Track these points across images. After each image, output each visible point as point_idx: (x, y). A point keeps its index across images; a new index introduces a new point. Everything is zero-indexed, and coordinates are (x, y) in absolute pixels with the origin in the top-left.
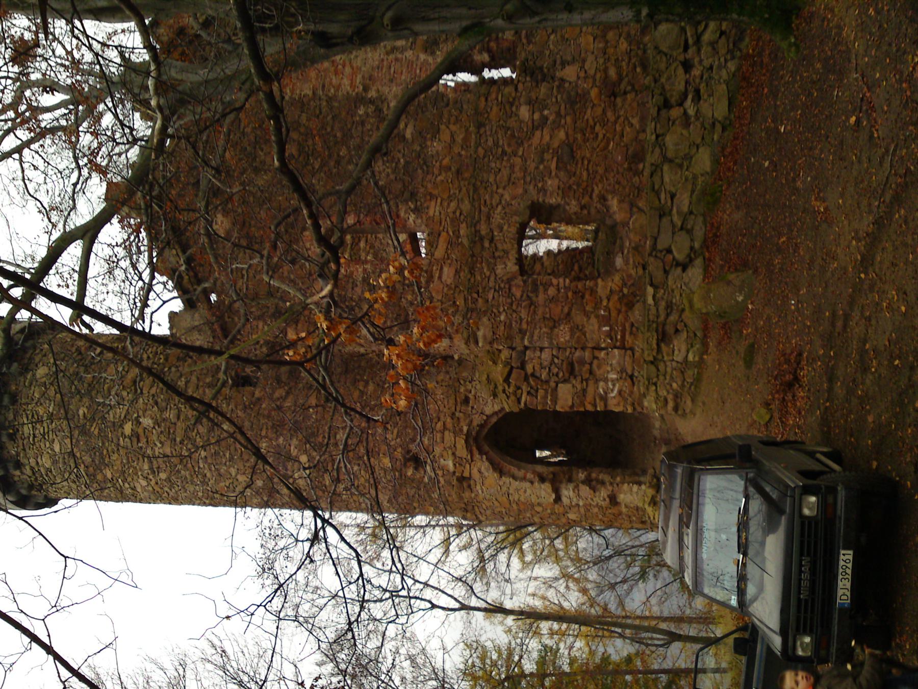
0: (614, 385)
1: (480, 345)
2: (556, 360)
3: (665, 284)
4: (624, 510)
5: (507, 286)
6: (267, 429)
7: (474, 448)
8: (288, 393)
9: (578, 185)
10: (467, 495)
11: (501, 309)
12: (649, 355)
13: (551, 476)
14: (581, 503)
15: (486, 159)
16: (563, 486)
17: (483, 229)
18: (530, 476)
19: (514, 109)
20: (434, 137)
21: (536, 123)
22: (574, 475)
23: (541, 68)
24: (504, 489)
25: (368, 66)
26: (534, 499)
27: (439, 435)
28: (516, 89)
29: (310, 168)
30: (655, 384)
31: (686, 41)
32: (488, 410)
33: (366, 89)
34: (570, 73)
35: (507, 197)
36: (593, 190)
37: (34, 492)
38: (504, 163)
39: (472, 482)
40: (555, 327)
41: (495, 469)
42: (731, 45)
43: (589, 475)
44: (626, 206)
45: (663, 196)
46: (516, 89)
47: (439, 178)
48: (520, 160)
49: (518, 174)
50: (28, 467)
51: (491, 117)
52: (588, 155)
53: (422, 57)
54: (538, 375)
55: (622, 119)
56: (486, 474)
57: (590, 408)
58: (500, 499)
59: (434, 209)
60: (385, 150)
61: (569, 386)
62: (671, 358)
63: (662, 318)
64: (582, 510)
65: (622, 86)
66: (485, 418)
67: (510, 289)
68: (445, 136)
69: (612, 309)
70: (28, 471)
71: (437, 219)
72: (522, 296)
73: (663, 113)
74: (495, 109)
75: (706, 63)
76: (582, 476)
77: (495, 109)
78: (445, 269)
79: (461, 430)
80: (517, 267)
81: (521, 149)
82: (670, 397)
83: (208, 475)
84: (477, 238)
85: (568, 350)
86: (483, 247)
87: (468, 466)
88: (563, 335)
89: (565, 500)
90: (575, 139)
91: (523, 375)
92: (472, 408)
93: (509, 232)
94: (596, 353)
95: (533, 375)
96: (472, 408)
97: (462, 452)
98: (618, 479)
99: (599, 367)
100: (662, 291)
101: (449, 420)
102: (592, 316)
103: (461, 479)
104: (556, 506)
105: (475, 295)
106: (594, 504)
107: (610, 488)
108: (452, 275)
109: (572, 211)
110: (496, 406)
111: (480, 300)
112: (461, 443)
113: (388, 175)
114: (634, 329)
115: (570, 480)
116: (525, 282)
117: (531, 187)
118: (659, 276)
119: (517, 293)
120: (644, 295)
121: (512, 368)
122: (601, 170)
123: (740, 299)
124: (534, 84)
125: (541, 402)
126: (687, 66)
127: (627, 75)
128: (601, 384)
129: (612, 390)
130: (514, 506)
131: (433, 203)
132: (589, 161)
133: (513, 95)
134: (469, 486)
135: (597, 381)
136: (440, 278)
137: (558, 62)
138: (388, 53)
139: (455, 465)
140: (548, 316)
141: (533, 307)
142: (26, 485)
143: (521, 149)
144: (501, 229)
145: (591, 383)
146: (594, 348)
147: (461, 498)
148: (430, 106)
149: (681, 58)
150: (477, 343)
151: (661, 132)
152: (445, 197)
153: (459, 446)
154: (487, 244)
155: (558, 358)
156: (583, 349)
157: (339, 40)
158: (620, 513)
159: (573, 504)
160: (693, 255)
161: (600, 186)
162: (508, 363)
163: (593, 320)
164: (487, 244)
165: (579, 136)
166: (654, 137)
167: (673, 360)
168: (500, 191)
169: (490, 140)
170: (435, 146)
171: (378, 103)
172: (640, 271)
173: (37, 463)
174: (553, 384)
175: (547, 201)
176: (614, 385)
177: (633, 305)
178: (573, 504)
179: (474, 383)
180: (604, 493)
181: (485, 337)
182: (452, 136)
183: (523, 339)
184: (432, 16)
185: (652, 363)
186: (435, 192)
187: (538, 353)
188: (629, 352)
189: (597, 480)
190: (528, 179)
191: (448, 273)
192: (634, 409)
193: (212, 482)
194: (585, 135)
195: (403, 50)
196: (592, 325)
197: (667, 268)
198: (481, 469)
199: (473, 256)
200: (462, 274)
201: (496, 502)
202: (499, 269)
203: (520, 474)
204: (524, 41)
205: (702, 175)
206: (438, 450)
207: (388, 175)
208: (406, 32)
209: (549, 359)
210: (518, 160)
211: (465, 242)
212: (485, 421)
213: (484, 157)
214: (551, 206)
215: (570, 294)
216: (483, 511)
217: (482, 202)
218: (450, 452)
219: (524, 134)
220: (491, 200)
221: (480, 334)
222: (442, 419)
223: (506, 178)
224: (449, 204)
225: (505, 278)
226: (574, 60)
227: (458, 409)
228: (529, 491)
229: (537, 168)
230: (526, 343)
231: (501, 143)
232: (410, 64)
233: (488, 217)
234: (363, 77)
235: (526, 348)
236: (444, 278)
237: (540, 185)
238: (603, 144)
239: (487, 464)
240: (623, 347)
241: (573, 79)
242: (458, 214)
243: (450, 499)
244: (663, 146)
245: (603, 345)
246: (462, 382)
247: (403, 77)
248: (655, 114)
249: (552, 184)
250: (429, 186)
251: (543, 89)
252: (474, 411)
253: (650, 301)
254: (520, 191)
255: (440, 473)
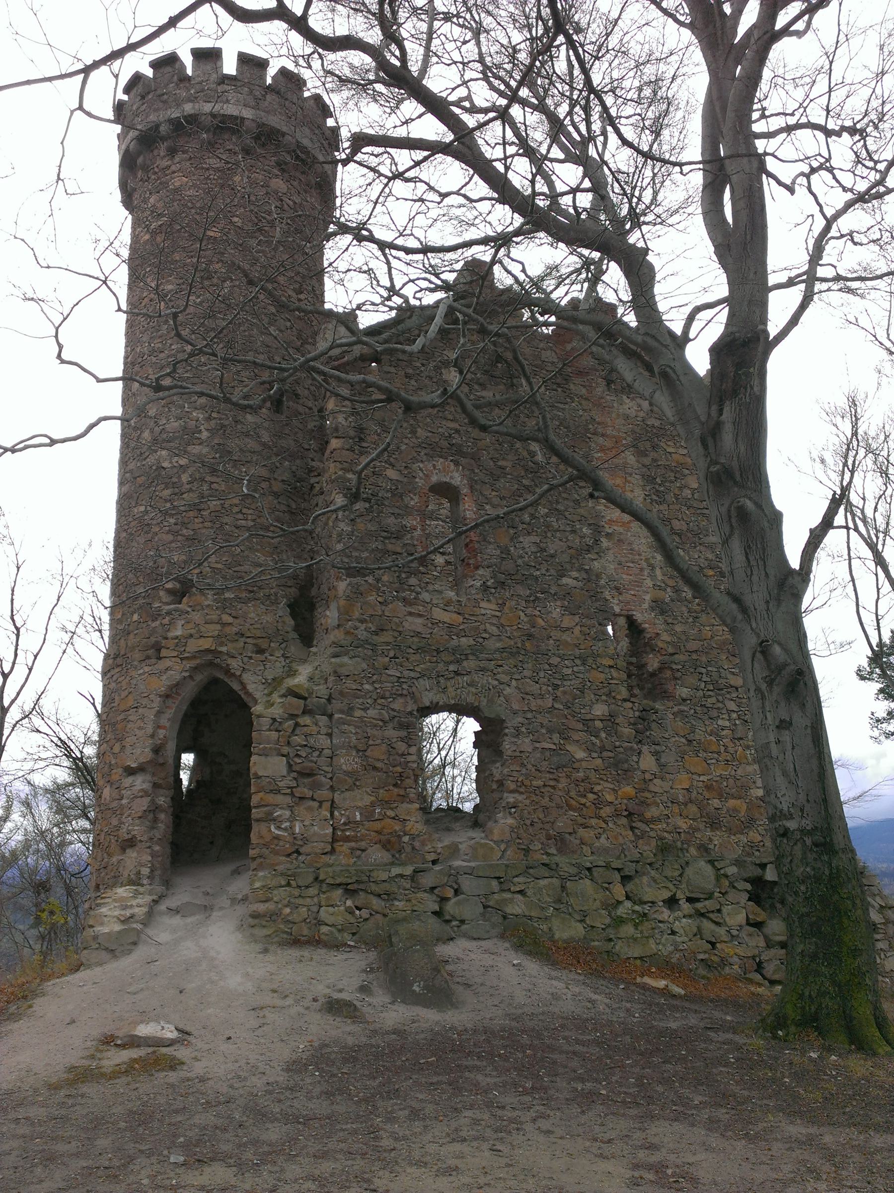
0: (285, 829)
1: (333, 660)
2: (316, 754)
3: (417, 888)
4: (114, 859)
5: (405, 692)
6: (220, 419)
7: (198, 661)
8: (264, 445)
9: (527, 776)
10: (137, 655)
11: (377, 686)
12: (327, 873)
13: (161, 761)
14: (124, 801)
15: (547, 667)
16: (148, 777)
17: (470, 664)
18: (162, 733)
19: (604, 698)
20: (566, 608)
21: (590, 723)
22: (162, 791)
23: (650, 729)
24: (145, 702)
25: (633, 539)
26: (129, 740)
27: (214, 617)
28: (625, 700)
29: (523, 474)
30: (289, 884)
31: (697, 900)
32: (247, 677)
33: (608, 535)
34: (648, 762)
35: (508, 691)
36: (522, 793)
37: (140, 174)
38: (544, 688)
39: (153, 661)
40: (358, 751)
41: (171, 688)
42: (701, 956)
43: (163, 811)
44: (507, 836)
45: (520, 879)
46: (625, 700)
47: (522, 614)
48: (550, 705)
49: (533, 705)
50: (169, 163)
51: (594, 672)
52: (560, 786)
53: (648, 597)
54: (297, 732)
55: (604, 825)
56: (164, 677)
57: (255, 800)
58: (130, 697)
59: (488, 608)
60: (596, 494)
61: (284, 772)
62: (323, 903)
63: (374, 887)
64: (114, 804)
65: (639, 824)
66: (238, 673)
67: (401, 695)
68: (567, 622)
69: (383, 823)
70: (165, 163)
71: (478, 611)
72: (393, 710)
73: (617, 876)
74: (602, 676)
75: (677, 926)
76: (162, 801)
77: (602, 676)
78: (419, 621)
79: (222, 644)
80: (428, 704)
81: (561, 707)
82: (270, 906)
83: (162, 355)
84: (460, 656)
85: (329, 769)
86: (449, 663)
87: (175, 654)
88: (347, 762)
89: (128, 781)
90: (577, 770)
91: (296, 713)
92: (251, 658)
93: (468, 694)
94: (327, 805)
95: (297, 725)
96: (251, 658)
97: (193, 646)
98: (157, 848)
99: (310, 809)
100: (408, 886)
101: (235, 629)
102: (373, 798)
103: (158, 647)
104: (120, 770)
105: (392, 654)
106: (123, 819)
107: (145, 838)
108: (413, 627)
109: (495, 771)
110: (254, 686)
111: (387, 659)
112: (206, 644)
113: (521, 557)
114: (359, 852)
115: (156, 786)
116: (411, 713)
117: (520, 719)
118: (427, 880)
119: (397, 705)
120: (403, 864)
121: (305, 699)
122: (545, 801)
123: (416, 988)
124: (632, 720)
125: (264, 735)
126: (672, 902)
127: (652, 829)
128: (288, 813)
129: (279, 828)
130: (122, 717)
131: (494, 607)
132: (553, 787)
133: (618, 697)
134: (148, 658)
135: (291, 808)
136: (410, 614)
137: (657, 748)
138: (647, 560)
139: (177, 638)
140: (371, 742)
141: (381, 723)
142: (148, 162)
143: (561, 707)
144: (471, 684)
145: (288, 799)
146: (333, 801)
147: (133, 649)
148: (597, 604)
149: (679, 895)
150: (336, 656)
151: (595, 874)
152: (503, 621)
153: (201, 642)
154: (452, 668)
155: (319, 756)
156: (332, 788)
157: (711, 449)
158: (110, 855)
159: (123, 792)
160: (454, 923)
161: (527, 802)
162: (311, 694)
163: (368, 800)
164: (452, 668)
165: (581, 774)
166: (588, 865)
167: (321, 907)
168: (514, 683)
169: (569, 671)
170: (555, 611)
171: (593, 548)
172: (432, 857)
173: (174, 172)
174: (285, 750)
175: (506, 738)
176: (285, 829)
177: (388, 850)
178: (123, 792)
179: (282, 659)
180: (138, 830)
181: (341, 665)
182: (568, 629)
183: (342, 712)
184: (751, 558)
185: (316, 879)
186: (506, 610)
187: (324, 730)
188: (329, 848)
189: (156, 820)
190: (529, 715)
191: (416, 624)
192: (254, 859)
193: (154, 359)
194: (583, 781)
195: (653, 577)
196: (362, 798)
197: (436, 891)
198: (173, 670)
199: (438, 651)
200: (416, 639)
201: (126, 692)
202: (424, 683)
203: (164, 721)
204: (676, 709)
205: (550, 929)
206: (196, 617)
207: (521, 557)
208: (727, 529)
209: (318, 746)
210: (549, 702)
211: (454, 642)
212: (233, 675)
213: (550, 665)
214: (499, 745)
215: (399, 769)
216: (115, 678)
217: (500, 663)
218: (193, 631)
219: (577, 710)
220: (503, 673)
221: (345, 659)
222: (237, 621)
223: (528, 689)
224: (494, 624)
225: (414, 689)
226: (662, 766)
227: (248, 640)
228: (140, 733)
229: (542, 726)
230: (336, 716)
231: (568, 683)
232: (639, 584)
233: (483, 669)
234: (621, 534)
235: (330, 716)
236: (410, 619)
237: (523, 729)
238: (574, 803)
239: (178, 677)
240: (334, 840)
241: (643, 765)
242: (484, 635)
243: (132, 636)
244: (578, 876)
245: (336, 813)
246: (283, 646)
247: (624, 576)
248: (614, 865)
249: (526, 743)
250: (514, 603)
251: (627, 731)
252: (246, 659)
253: (396, 871)
254: (516, 707)
255: (166, 621)
